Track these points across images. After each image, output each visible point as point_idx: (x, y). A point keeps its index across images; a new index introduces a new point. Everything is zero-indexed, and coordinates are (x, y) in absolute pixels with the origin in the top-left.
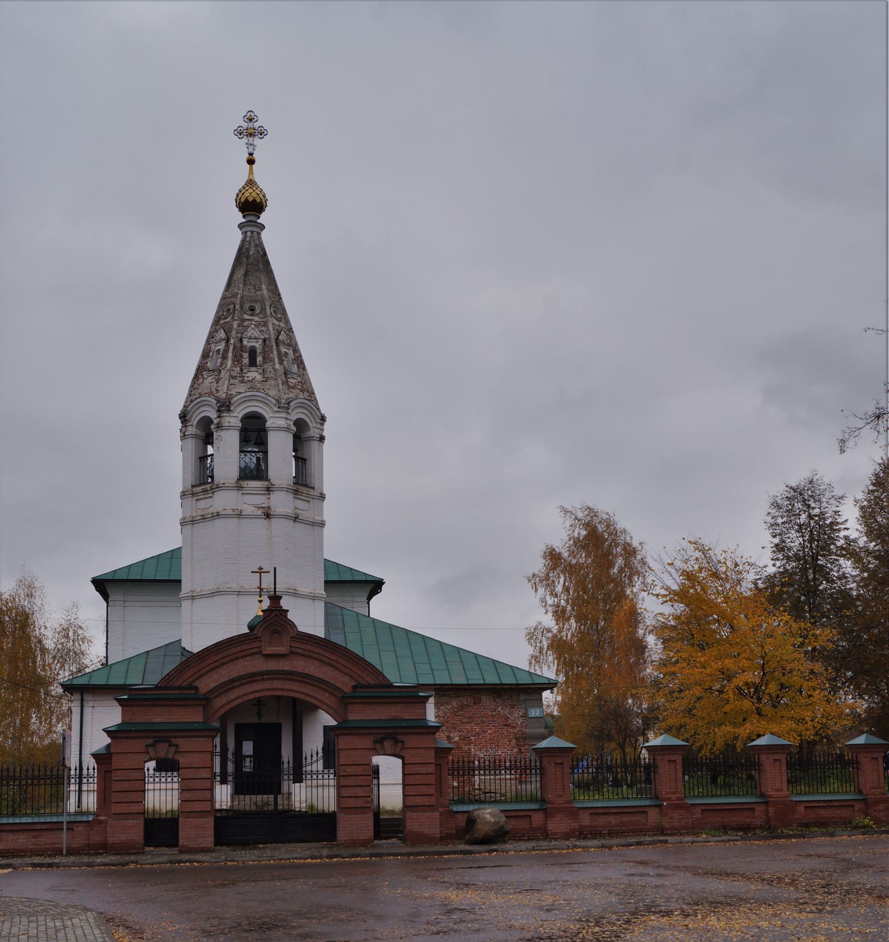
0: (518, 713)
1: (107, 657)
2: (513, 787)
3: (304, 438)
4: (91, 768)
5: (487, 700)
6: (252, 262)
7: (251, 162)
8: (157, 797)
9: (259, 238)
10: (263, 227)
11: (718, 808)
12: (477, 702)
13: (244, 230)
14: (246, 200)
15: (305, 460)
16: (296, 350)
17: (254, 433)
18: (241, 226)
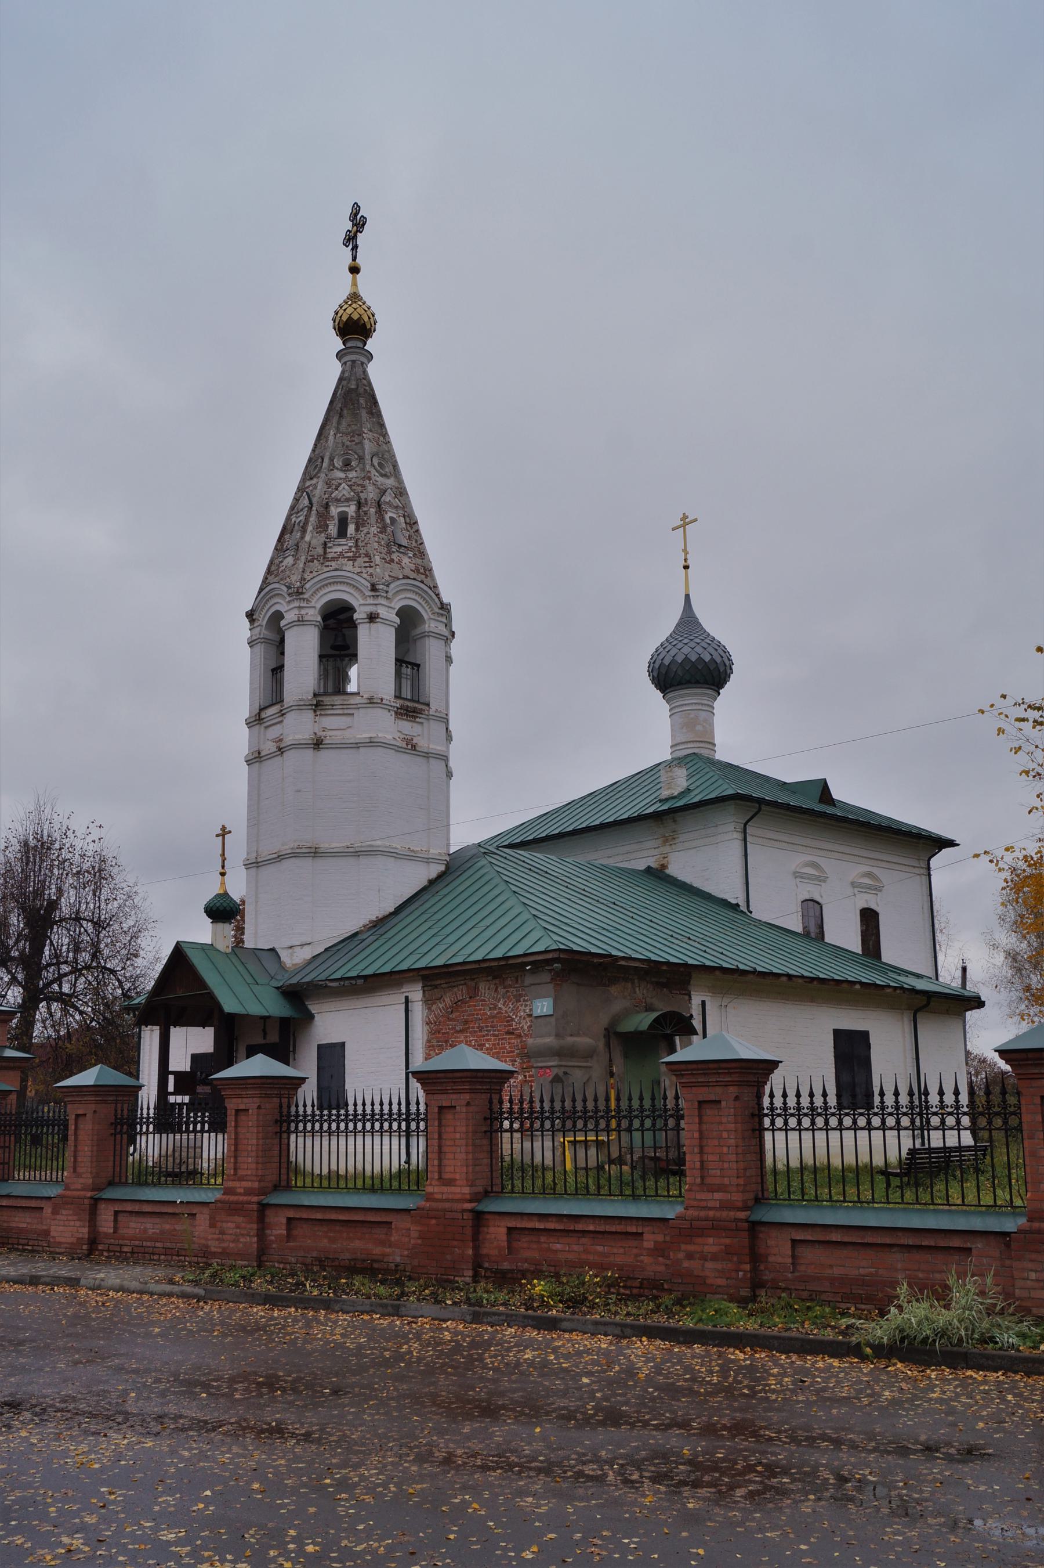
2: (517, 1146)
4: (309, 1103)
6: (354, 403)
7: (354, 270)
8: (794, 1143)
9: (365, 372)
11: (319, 1216)
12: (474, 993)
13: (343, 361)
14: (350, 318)
15: (418, 666)
17: (339, 634)
18: (339, 355)
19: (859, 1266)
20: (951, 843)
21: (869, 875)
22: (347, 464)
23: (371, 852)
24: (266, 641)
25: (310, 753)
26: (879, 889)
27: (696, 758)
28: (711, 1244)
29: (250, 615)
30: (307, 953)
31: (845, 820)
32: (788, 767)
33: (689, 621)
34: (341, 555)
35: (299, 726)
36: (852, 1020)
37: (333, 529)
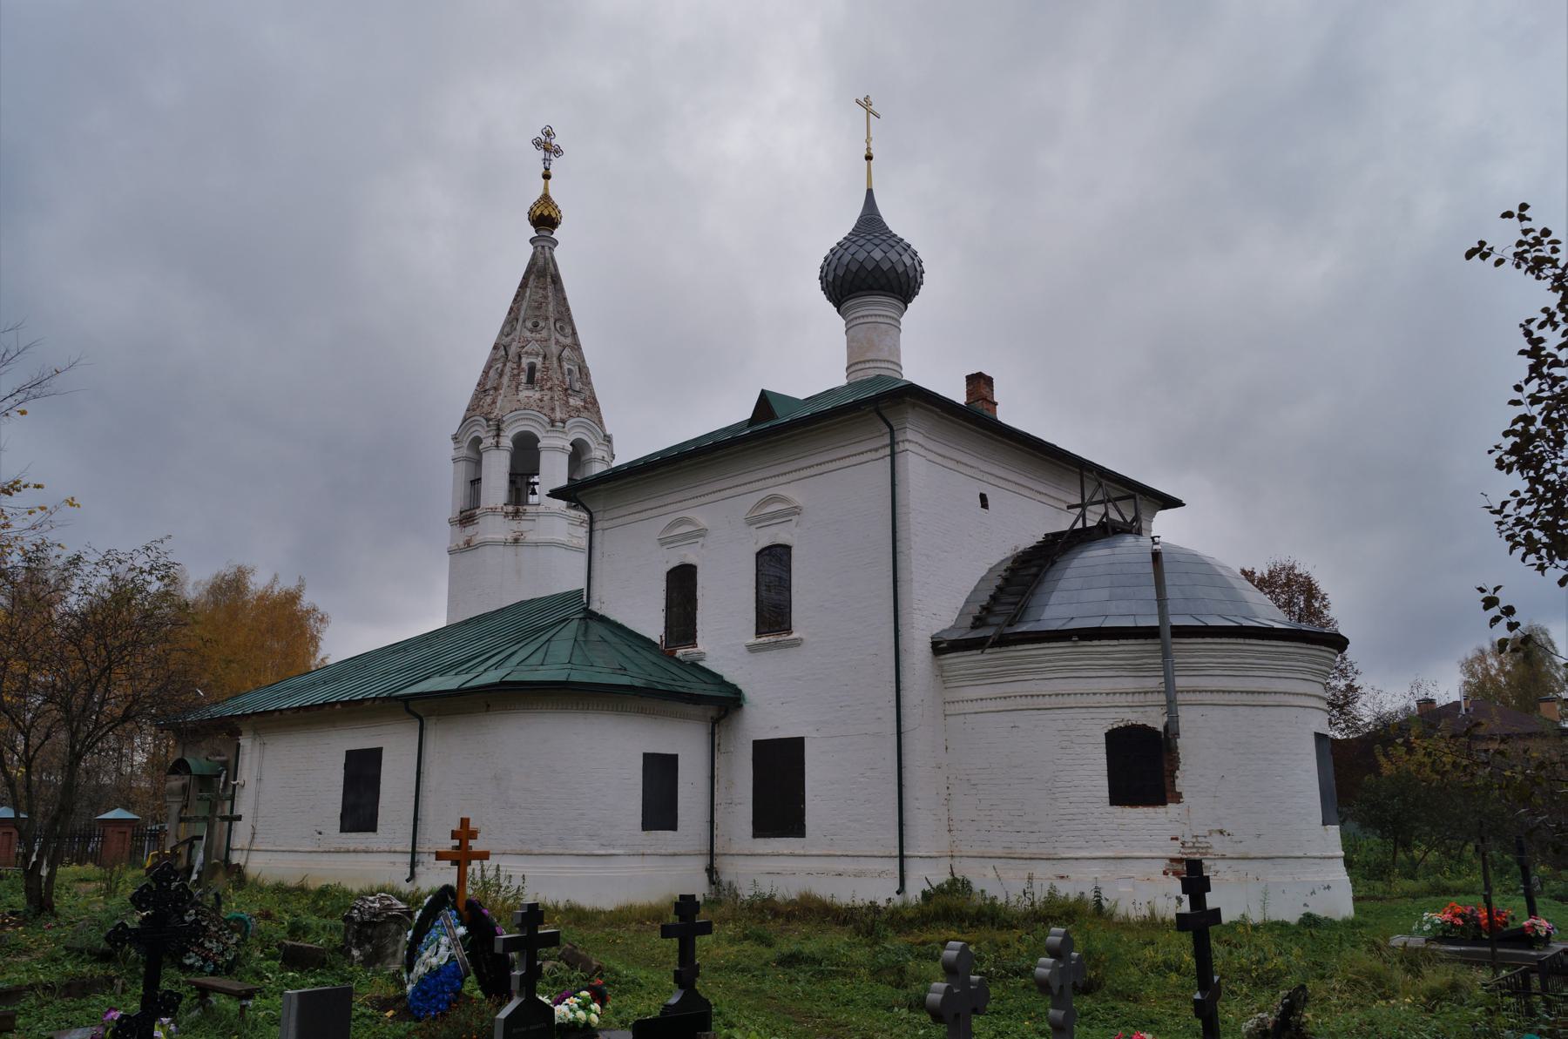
1: (1223, 857)
6: (542, 276)
7: (547, 176)
10: (555, 243)
18: (532, 241)
20: (1177, 503)
24: (467, 459)
25: (510, 550)
29: (455, 438)
33: (870, 220)
36: (362, 739)
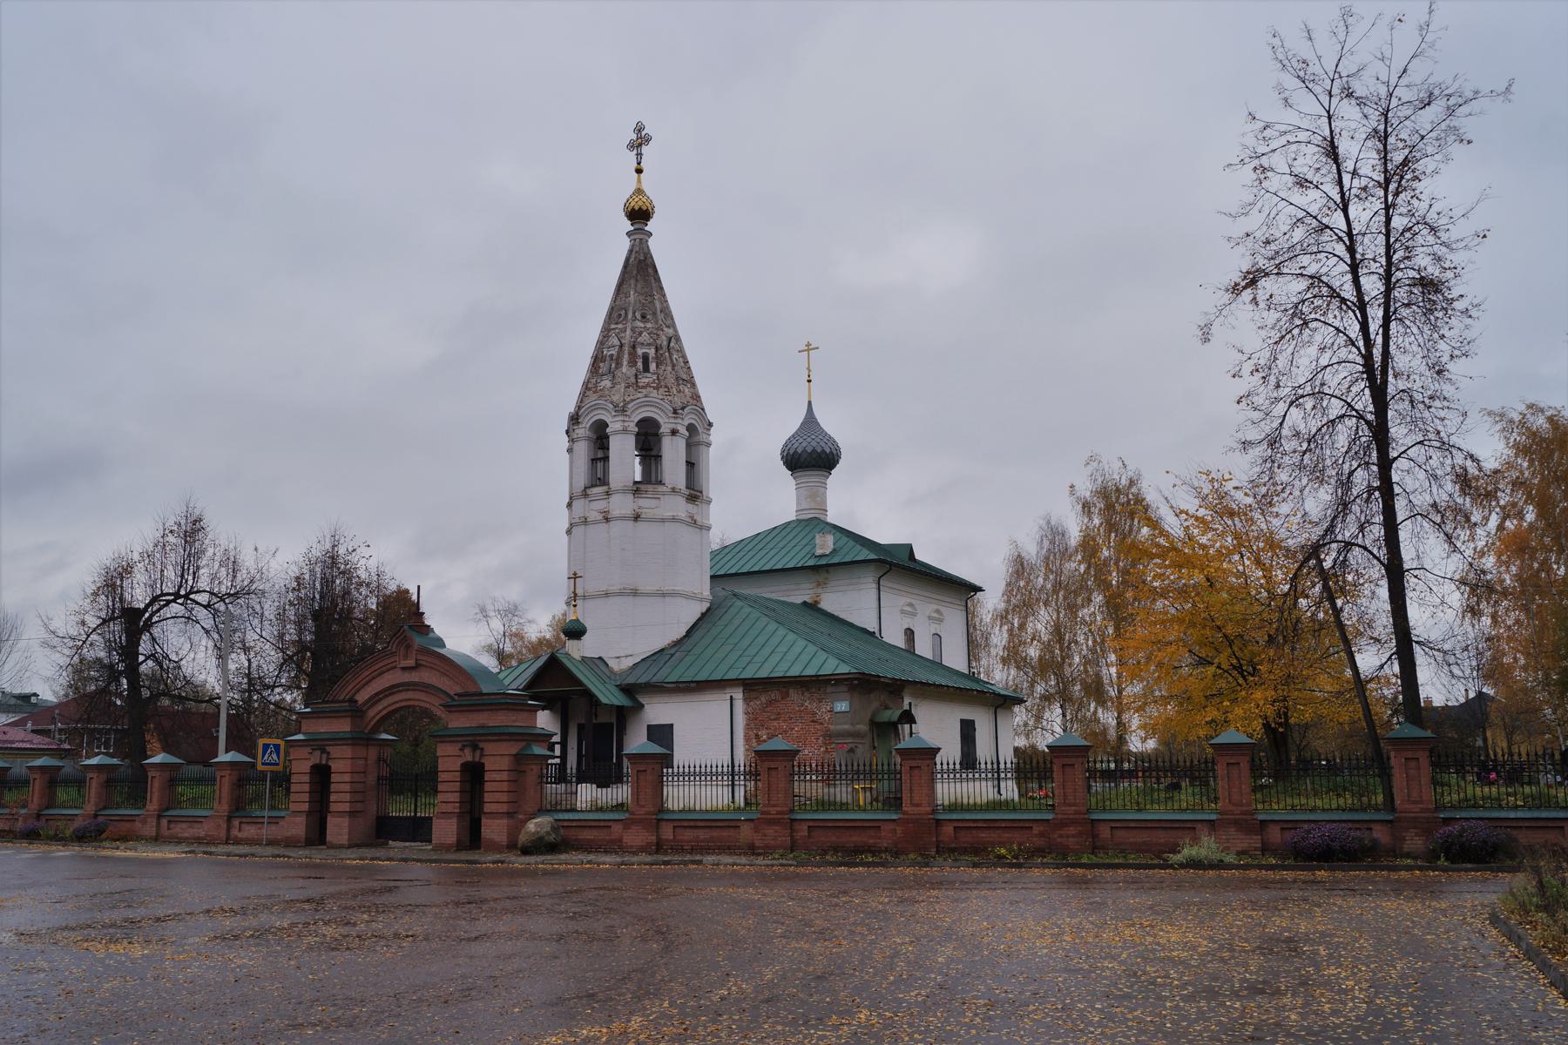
0: (825, 708)
3: (695, 439)
5: (794, 695)
6: (640, 270)
7: (639, 171)
12: (785, 696)
16: (684, 357)
19: (1162, 837)
21: (911, 605)
22: (643, 317)
23: (674, 594)
25: (631, 523)
26: (941, 621)
27: (813, 523)
28: (1072, 830)
30: (629, 662)
31: (920, 572)
32: (885, 533)
33: (810, 421)
34: (648, 385)
35: (621, 505)
36: (968, 713)
37: (640, 365)
